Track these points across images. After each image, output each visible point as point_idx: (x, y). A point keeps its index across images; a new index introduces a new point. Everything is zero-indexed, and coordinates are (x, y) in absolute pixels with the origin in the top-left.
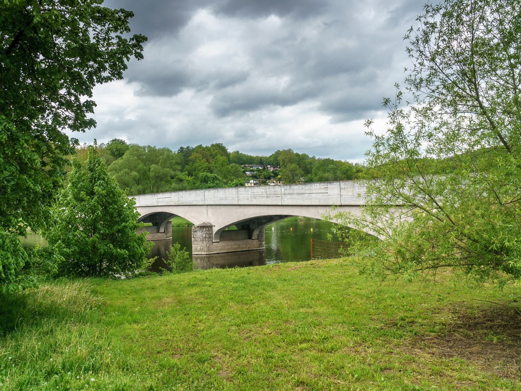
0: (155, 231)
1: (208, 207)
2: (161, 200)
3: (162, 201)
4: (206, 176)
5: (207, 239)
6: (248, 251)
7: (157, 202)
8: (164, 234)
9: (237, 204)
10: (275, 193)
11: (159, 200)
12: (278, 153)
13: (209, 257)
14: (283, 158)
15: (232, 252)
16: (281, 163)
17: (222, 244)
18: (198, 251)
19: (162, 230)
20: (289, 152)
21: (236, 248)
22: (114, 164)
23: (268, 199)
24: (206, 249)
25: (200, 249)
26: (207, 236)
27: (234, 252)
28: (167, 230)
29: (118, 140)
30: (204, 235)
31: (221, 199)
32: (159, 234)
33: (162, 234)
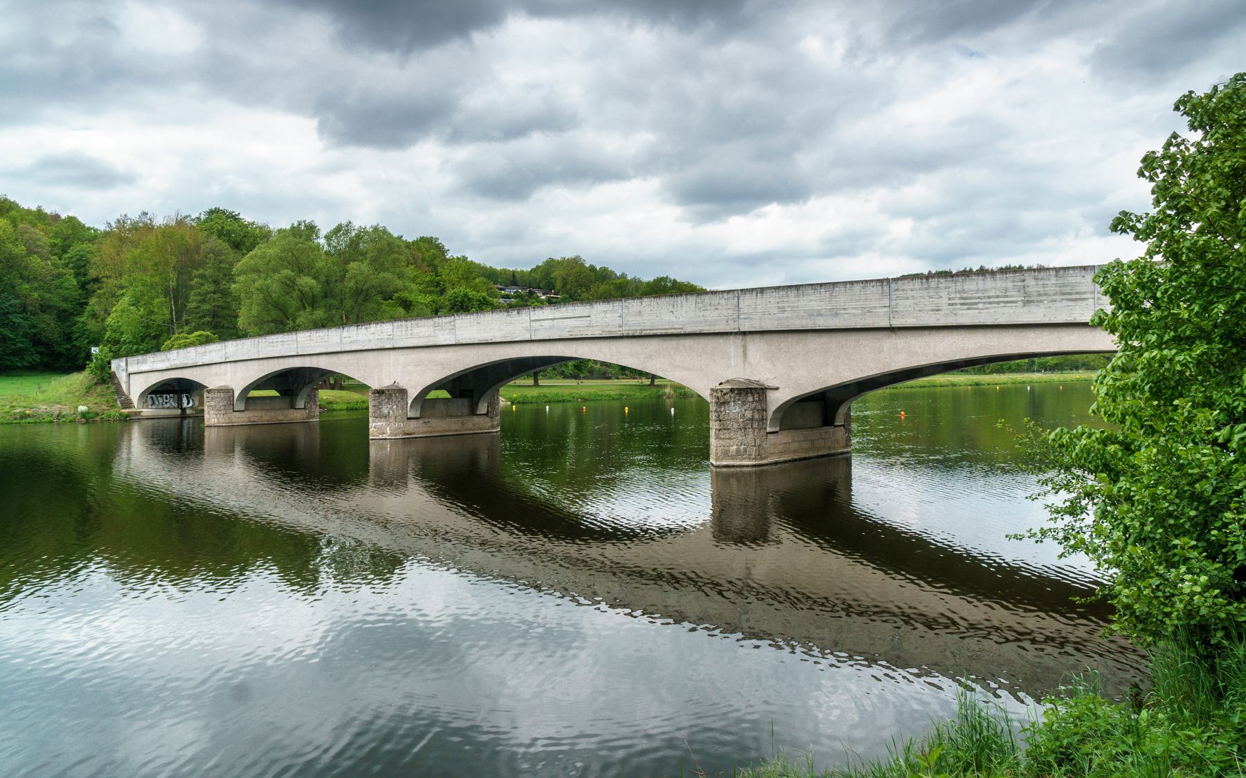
0: (466, 410)
1: (749, 338)
2: (546, 324)
3: (551, 327)
4: (466, 295)
5: (755, 425)
6: (828, 455)
7: (529, 330)
8: (488, 419)
9: (885, 324)
10: (1068, 290)
11: (534, 324)
12: (551, 264)
13: (762, 471)
14: (563, 273)
15: (801, 459)
16: (559, 285)
17: (784, 437)
18: (732, 457)
19: (483, 409)
20: (575, 263)
21: (808, 450)
22: (252, 258)
23: (1033, 308)
24: (753, 451)
25: (738, 451)
26: (756, 417)
27: (805, 459)
28: (493, 408)
29: (224, 212)
30: (749, 414)
31: (812, 314)
32: (476, 419)
33: (481, 419)
